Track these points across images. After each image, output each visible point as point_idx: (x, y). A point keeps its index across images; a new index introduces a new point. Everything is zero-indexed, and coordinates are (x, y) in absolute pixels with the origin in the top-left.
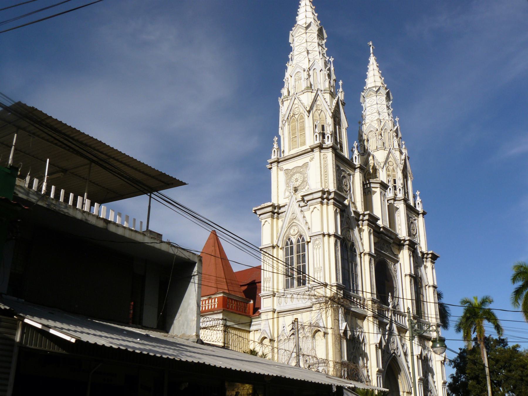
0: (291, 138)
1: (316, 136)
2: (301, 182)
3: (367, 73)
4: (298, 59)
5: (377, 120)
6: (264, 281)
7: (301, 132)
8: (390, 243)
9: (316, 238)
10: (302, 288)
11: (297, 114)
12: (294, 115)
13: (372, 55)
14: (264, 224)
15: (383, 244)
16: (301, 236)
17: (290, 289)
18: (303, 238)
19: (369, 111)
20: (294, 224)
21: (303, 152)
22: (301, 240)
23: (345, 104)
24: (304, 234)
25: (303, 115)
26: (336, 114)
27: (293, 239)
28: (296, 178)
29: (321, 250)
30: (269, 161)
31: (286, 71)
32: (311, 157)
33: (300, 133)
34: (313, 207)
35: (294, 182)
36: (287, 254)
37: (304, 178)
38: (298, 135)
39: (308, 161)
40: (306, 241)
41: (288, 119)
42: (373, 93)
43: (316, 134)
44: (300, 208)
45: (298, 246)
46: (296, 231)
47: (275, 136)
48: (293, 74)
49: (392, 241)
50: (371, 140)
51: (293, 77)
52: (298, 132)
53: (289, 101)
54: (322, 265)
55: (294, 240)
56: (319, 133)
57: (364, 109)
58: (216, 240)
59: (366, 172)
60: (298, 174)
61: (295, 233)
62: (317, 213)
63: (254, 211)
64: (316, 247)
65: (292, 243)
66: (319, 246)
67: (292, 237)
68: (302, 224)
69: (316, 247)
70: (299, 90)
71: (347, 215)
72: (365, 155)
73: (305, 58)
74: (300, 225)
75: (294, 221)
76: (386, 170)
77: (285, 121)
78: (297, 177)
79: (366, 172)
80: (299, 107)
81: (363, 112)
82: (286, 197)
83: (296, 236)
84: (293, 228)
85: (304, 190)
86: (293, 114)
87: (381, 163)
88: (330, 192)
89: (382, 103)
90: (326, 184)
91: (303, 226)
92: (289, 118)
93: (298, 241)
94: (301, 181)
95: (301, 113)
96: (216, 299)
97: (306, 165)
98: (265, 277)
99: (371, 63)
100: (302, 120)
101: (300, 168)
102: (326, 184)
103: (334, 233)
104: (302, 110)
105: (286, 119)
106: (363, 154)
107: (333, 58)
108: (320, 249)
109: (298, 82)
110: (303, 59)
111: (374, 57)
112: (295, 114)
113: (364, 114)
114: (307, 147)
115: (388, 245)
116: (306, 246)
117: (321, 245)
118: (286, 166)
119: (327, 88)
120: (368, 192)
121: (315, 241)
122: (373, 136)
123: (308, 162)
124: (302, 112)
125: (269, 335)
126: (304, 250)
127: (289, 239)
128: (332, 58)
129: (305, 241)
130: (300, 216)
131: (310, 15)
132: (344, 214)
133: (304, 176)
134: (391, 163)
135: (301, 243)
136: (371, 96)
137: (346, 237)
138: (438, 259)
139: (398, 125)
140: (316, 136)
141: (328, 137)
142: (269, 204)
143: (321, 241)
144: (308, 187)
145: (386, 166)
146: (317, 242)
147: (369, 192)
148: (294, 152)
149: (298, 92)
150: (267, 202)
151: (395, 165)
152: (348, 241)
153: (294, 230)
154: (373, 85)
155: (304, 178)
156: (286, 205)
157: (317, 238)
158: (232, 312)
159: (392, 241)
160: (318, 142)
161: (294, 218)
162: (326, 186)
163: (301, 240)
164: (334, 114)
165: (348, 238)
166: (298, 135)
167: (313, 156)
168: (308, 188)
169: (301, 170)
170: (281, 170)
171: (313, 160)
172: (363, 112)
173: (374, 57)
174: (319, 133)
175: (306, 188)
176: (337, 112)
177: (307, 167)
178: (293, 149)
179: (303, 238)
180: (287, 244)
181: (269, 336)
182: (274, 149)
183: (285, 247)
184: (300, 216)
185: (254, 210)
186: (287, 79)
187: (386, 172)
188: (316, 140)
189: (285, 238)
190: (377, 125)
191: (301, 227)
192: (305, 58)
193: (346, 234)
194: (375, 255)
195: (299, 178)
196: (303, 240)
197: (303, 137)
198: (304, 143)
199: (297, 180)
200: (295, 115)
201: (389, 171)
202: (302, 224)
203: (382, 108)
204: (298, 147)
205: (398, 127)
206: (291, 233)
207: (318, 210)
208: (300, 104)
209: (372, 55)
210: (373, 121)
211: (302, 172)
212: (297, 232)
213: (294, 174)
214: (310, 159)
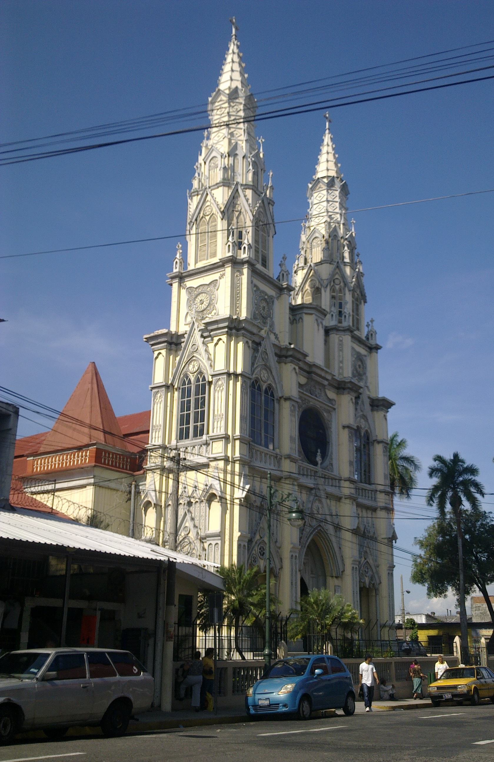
0: (210, 242)
1: (229, 246)
2: (207, 304)
3: (319, 157)
4: (216, 138)
5: (325, 222)
6: (152, 429)
7: (212, 240)
8: (324, 386)
9: (218, 378)
10: (199, 439)
11: (209, 215)
12: (204, 216)
13: (327, 131)
14: (157, 358)
15: (314, 386)
16: (201, 373)
17: (184, 440)
18: (204, 376)
19: (316, 209)
20: (194, 358)
21: (212, 267)
22: (201, 380)
23: (274, 203)
24: (205, 371)
25: (215, 216)
26: (259, 217)
27: (192, 377)
28: (201, 299)
29: (224, 393)
30: (169, 275)
31: (199, 153)
32: (221, 273)
33: (211, 240)
34: (218, 338)
35: (199, 304)
36: (183, 397)
37: (211, 300)
38: (208, 243)
39: (218, 278)
40: (207, 380)
41: (196, 220)
42: (322, 186)
43: (229, 243)
44: (203, 339)
45: (197, 387)
46: (196, 368)
47: (179, 243)
48: (207, 159)
49: (326, 383)
50: (315, 249)
51: (207, 163)
52: (208, 239)
53: (199, 196)
54: (223, 412)
55: (192, 379)
56: (232, 243)
57: (311, 206)
58: (94, 374)
59: (306, 291)
60: (204, 294)
61: (195, 370)
62: (222, 346)
63: (145, 340)
64: (218, 389)
65: (190, 382)
66: (221, 388)
67: (191, 375)
68: (203, 358)
69: (218, 389)
70: (212, 183)
71: (263, 349)
72: (305, 269)
73: (224, 138)
74: (201, 361)
75: (195, 355)
76: (330, 290)
77: (192, 224)
78: (203, 299)
79: (306, 291)
80: (211, 205)
81: (309, 210)
82: (187, 323)
83: (195, 374)
84: (193, 363)
85: (210, 316)
86: (203, 214)
87: (325, 281)
88: (172, 334)
89: (335, 200)
90: (238, 309)
91: (204, 361)
92: (199, 219)
93: (198, 380)
94: (207, 303)
95: (213, 214)
96: (88, 452)
97: (214, 282)
98: (154, 424)
99: (325, 143)
100: (214, 224)
101: (206, 287)
102: (238, 309)
103: (242, 372)
104: (215, 210)
105: (193, 220)
106: (303, 267)
107: (263, 139)
108: (223, 392)
109: (213, 170)
110: (222, 139)
111: (330, 135)
112: (206, 215)
113: (310, 212)
114: (215, 260)
115: (320, 388)
116: (207, 387)
117: (224, 387)
118: (192, 283)
119: (250, 181)
120: (299, 320)
121: (217, 382)
122: (318, 244)
123: (217, 280)
124: (214, 213)
125: (154, 498)
126: (204, 393)
127: (187, 377)
128: (263, 138)
129: (205, 381)
130: (202, 348)
131: (237, 76)
132: (259, 348)
133: (210, 298)
134: (337, 282)
135: (201, 383)
136: (320, 189)
137: (259, 377)
138: (393, 407)
139: (353, 230)
140: (229, 246)
141: (245, 248)
142: (165, 331)
143: (224, 382)
144: (214, 311)
145: (330, 285)
146: (220, 383)
147: (301, 320)
148: (200, 265)
149: (213, 184)
150: (162, 329)
151: (342, 284)
152: (263, 382)
153: (194, 367)
154: (324, 174)
155: (211, 300)
156: (186, 333)
157: (220, 377)
158: (107, 469)
159: (326, 383)
160: (230, 254)
161: (195, 350)
162: (238, 312)
163: (201, 380)
164: (257, 216)
165: (263, 379)
166: (208, 243)
167: (224, 272)
168: (215, 314)
169: (208, 290)
170: (184, 288)
171: (223, 278)
172: (309, 210)
173: (330, 135)
174: (232, 243)
175: (213, 313)
176: (261, 214)
177: (215, 286)
178: (200, 261)
179: (204, 377)
180: (184, 384)
181: (153, 500)
182: (177, 260)
183: (181, 387)
184: (202, 348)
185: (145, 338)
186: (199, 166)
187: (330, 293)
188: (229, 251)
189: (182, 376)
190: (324, 229)
191: (202, 362)
192: (224, 138)
193: (260, 374)
194: (299, 401)
195: (205, 300)
196: (204, 379)
197: (213, 245)
198: (214, 255)
199: (202, 302)
200: (205, 216)
201: (334, 291)
202: (203, 358)
203: (333, 207)
204: (207, 259)
205: (352, 233)
206: (190, 370)
207: (224, 342)
208: (212, 201)
209: (327, 131)
210: (320, 224)
211: (208, 291)
212: (197, 369)
213: (199, 294)
214: (220, 275)
